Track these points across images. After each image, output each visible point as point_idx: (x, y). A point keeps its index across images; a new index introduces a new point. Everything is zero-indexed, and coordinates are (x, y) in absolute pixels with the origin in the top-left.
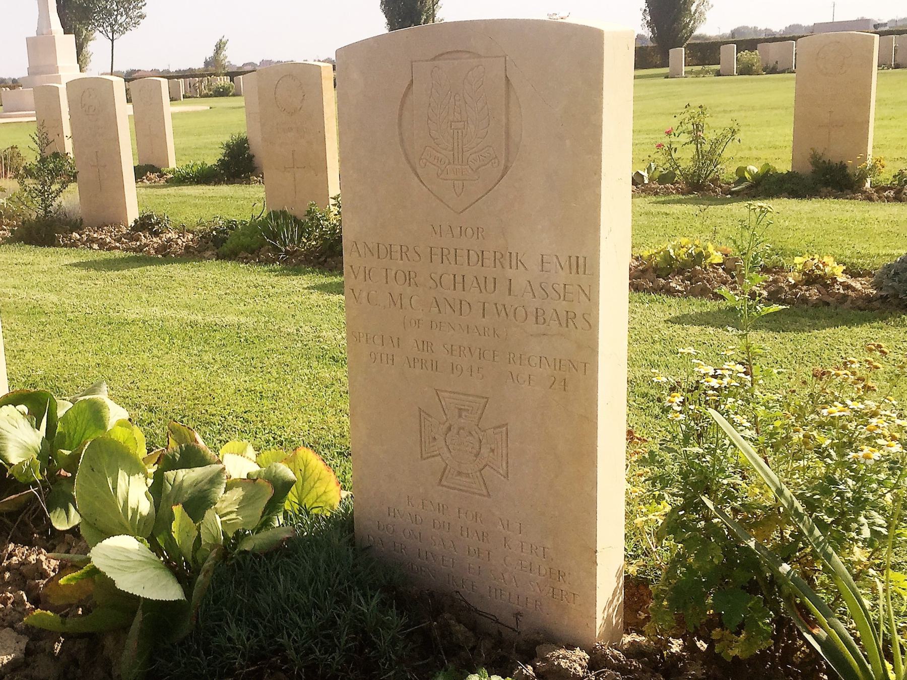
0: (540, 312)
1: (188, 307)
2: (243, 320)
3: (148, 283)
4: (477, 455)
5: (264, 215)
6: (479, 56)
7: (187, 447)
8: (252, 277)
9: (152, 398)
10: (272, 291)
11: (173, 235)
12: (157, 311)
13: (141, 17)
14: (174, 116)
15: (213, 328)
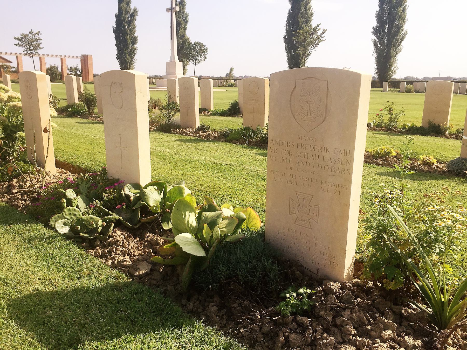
0: (333, 168)
1: (214, 157)
2: (232, 163)
3: (201, 148)
4: (308, 215)
5: (242, 128)
6: (319, 80)
7: (210, 204)
8: (236, 149)
9: (200, 187)
10: (243, 154)
11: (211, 133)
12: (204, 158)
13: (206, 58)
14: (214, 92)
15: (222, 165)
